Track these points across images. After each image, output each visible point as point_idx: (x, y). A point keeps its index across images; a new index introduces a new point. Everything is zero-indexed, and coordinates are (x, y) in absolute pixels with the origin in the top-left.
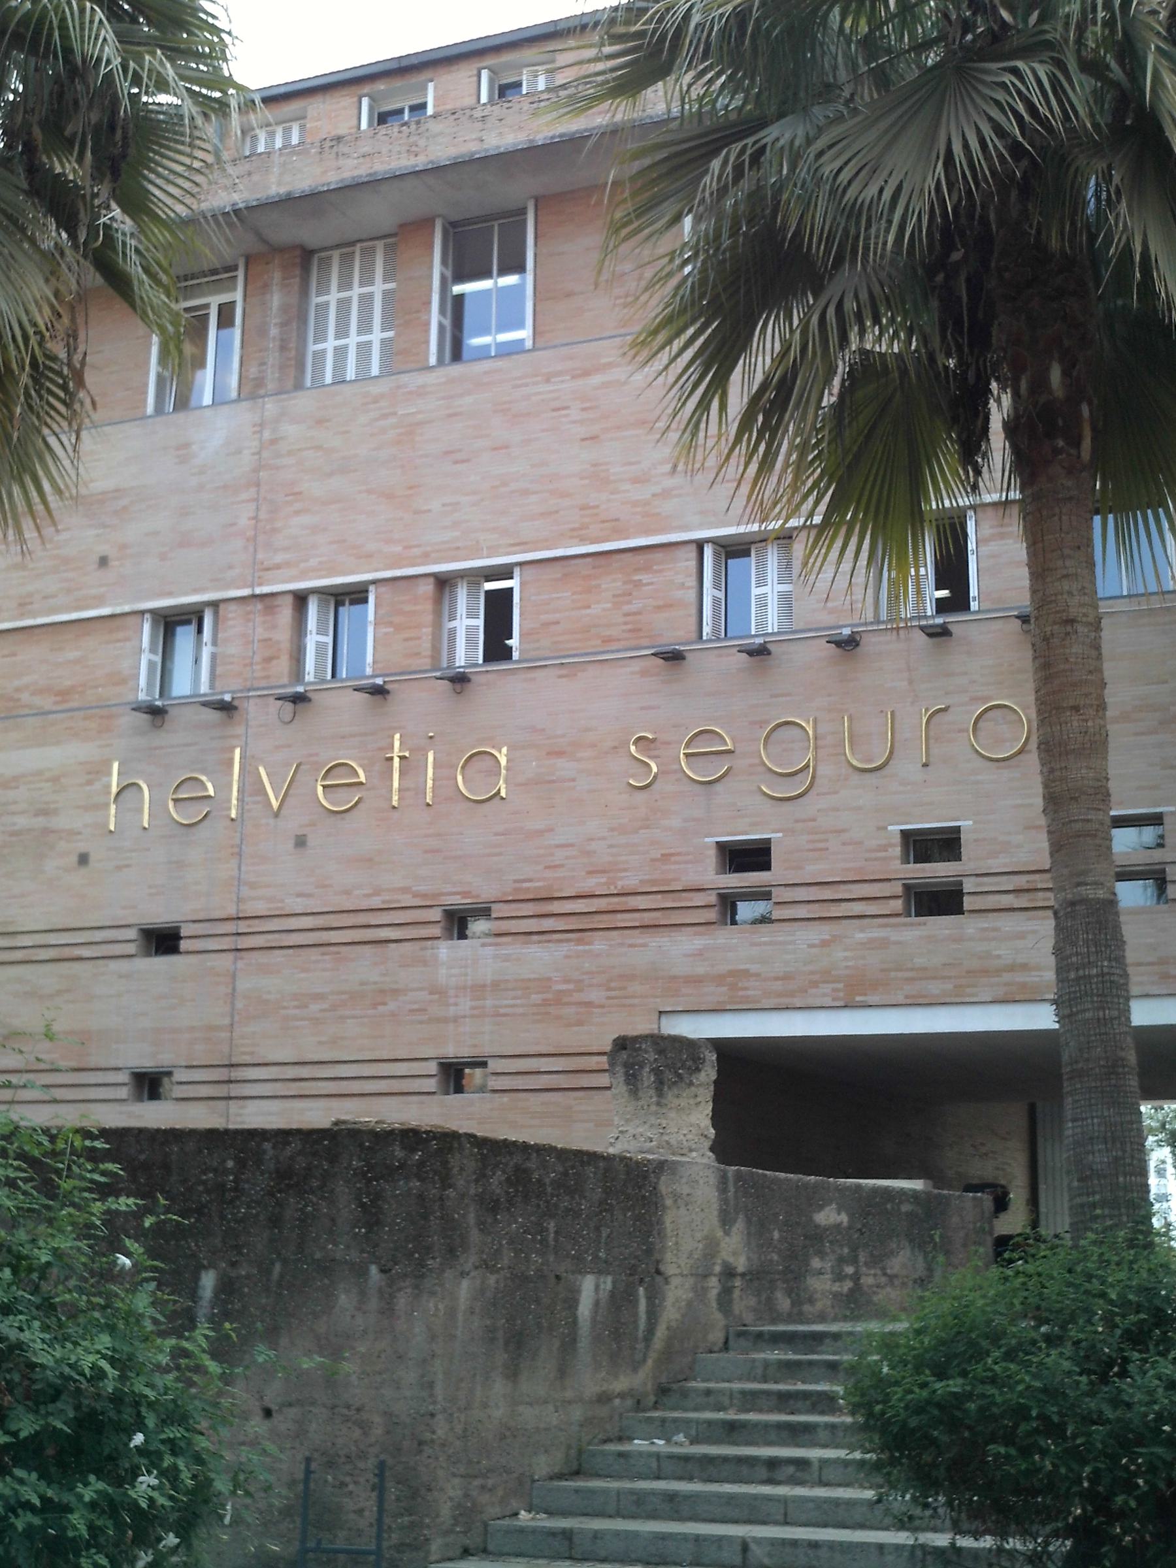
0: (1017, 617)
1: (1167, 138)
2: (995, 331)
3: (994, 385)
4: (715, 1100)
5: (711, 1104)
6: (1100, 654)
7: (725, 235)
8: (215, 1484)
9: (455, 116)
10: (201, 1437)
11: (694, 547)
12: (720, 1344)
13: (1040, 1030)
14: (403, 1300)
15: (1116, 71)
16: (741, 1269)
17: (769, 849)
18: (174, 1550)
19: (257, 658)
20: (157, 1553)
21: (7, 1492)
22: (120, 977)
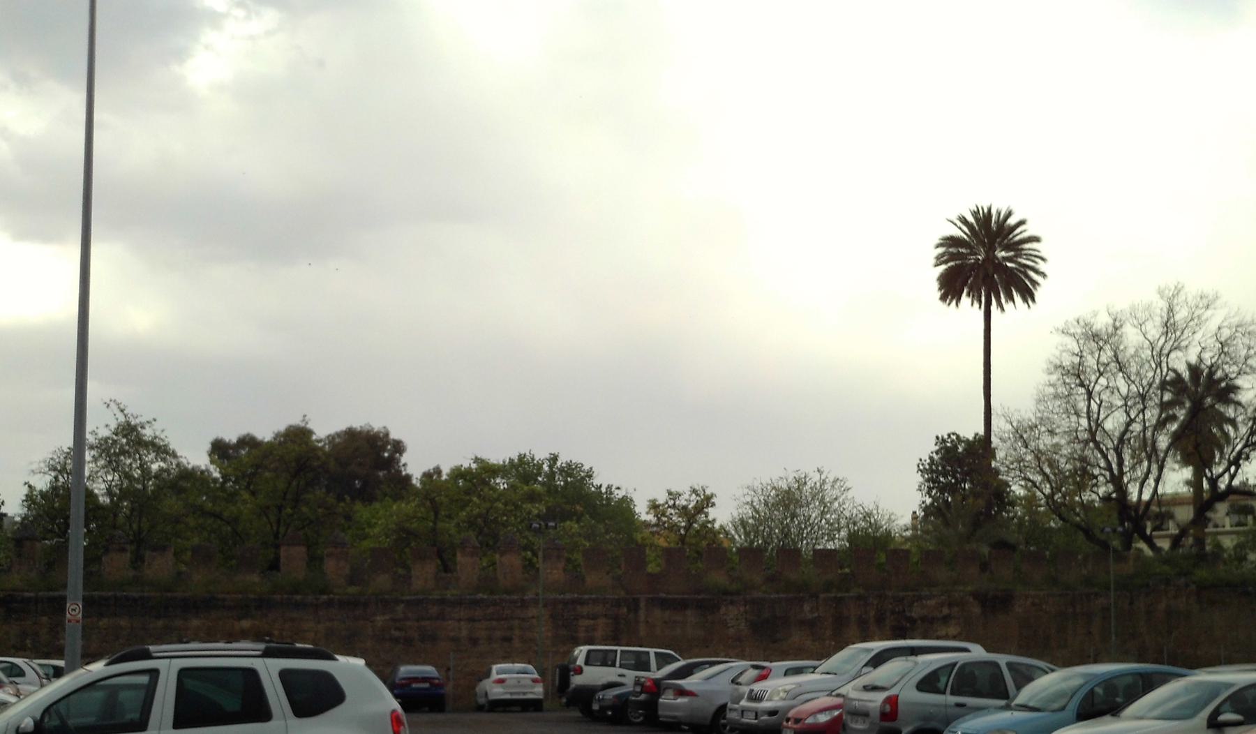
12: (745, 713)
17: (64, 648)
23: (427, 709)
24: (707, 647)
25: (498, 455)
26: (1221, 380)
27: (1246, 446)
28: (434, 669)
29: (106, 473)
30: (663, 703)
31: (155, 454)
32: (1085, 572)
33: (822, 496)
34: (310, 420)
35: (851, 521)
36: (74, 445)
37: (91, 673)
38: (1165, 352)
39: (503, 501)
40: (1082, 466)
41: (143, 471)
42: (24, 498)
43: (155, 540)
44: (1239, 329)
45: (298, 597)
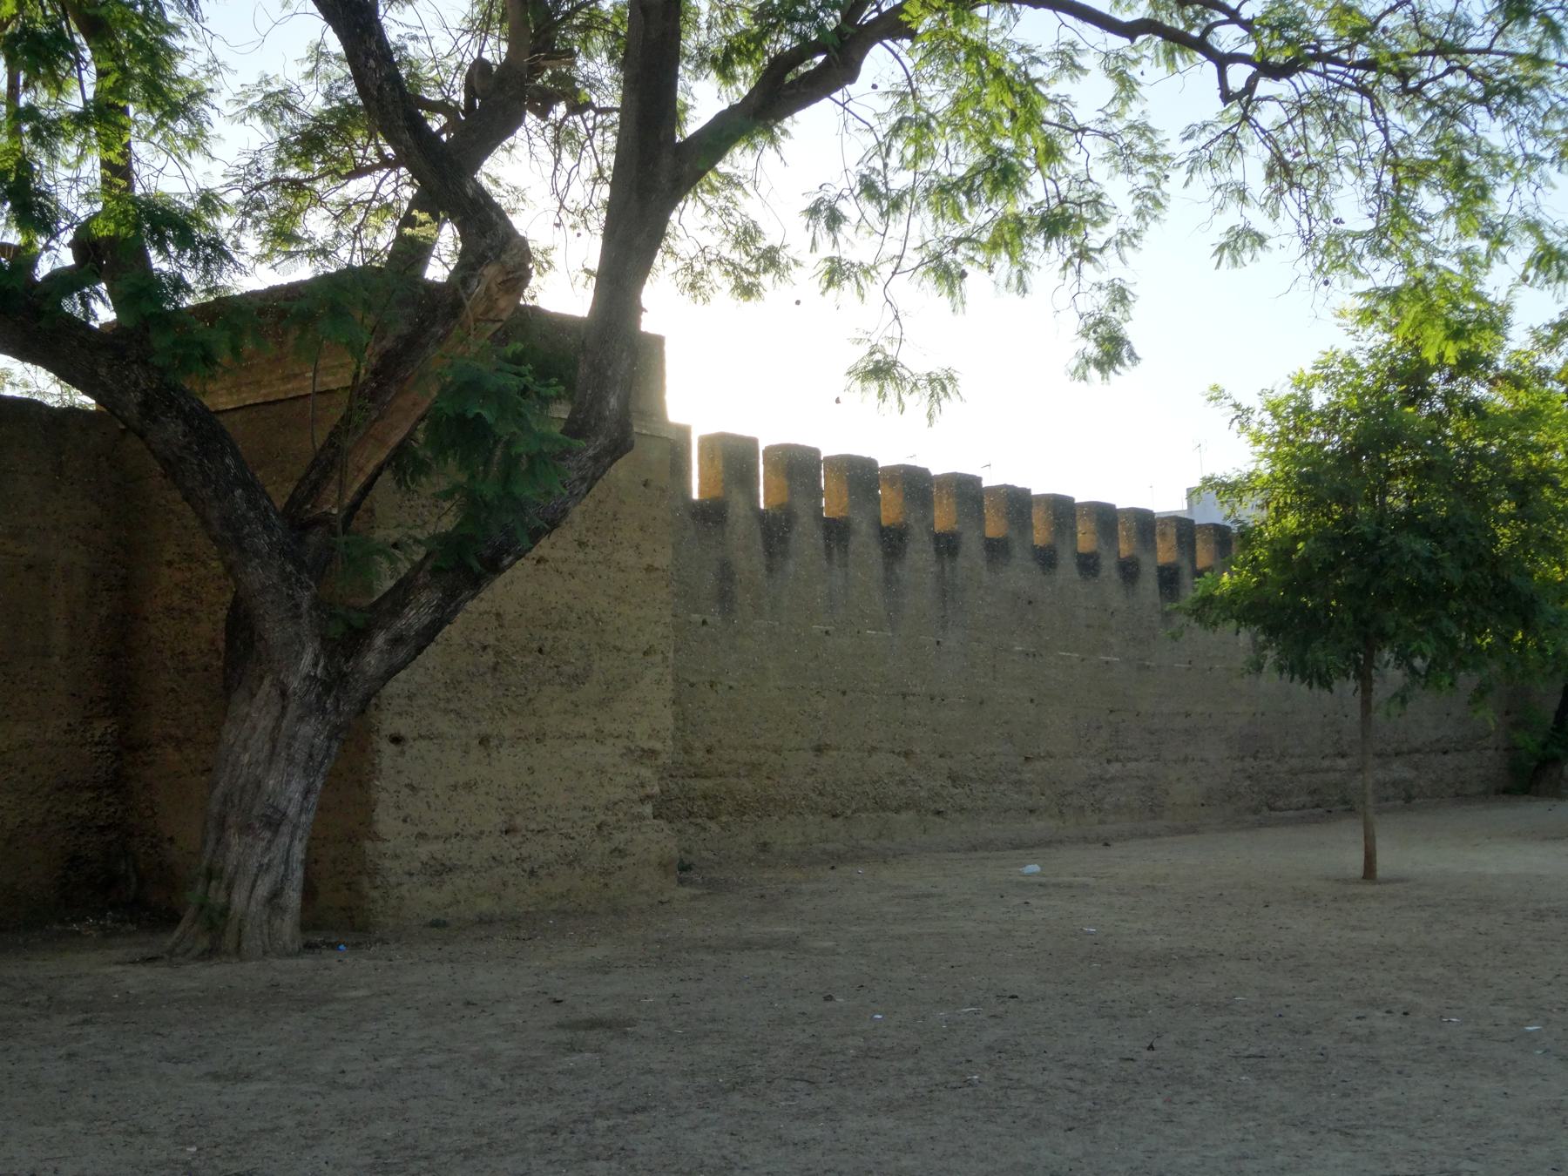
0: (828, 286)
1: (242, 296)
2: (435, 394)
3: (360, 102)
4: (732, 108)
5: (1560, 698)
6: (1256, 234)
7: (708, 783)
8: (1040, 544)
9: (585, 813)
10: (517, 1122)
11: (1380, 873)
12: (1359, 872)
13: (966, 475)
14: (1320, 655)
15: (1081, 371)
16: (323, 212)
18: (1524, 640)
19: (432, 1125)
20: (1439, 428)
21: (1564, 55)
22: (302, 1094)
23: (516, 240)
24: (833, 868)
25: (1040, 485)
26: (1309, 492)
27: (1449, 483)
28: (93, 402)
29: (374, 901)
30: (701, 492)
31: (1004, 256)
32: (103, 611)
33: (167, 251)
34: (958, 303)
35: (1393, 248)
36: (535, 309)
37: (509, 11)
38: (554, 1157)
39: (1465, 346)
40: (1461, 351)
41: (559, 52)
42: (465, 26)
43: (335, 511)
44: (910, 784)
45: (1531, 146)
